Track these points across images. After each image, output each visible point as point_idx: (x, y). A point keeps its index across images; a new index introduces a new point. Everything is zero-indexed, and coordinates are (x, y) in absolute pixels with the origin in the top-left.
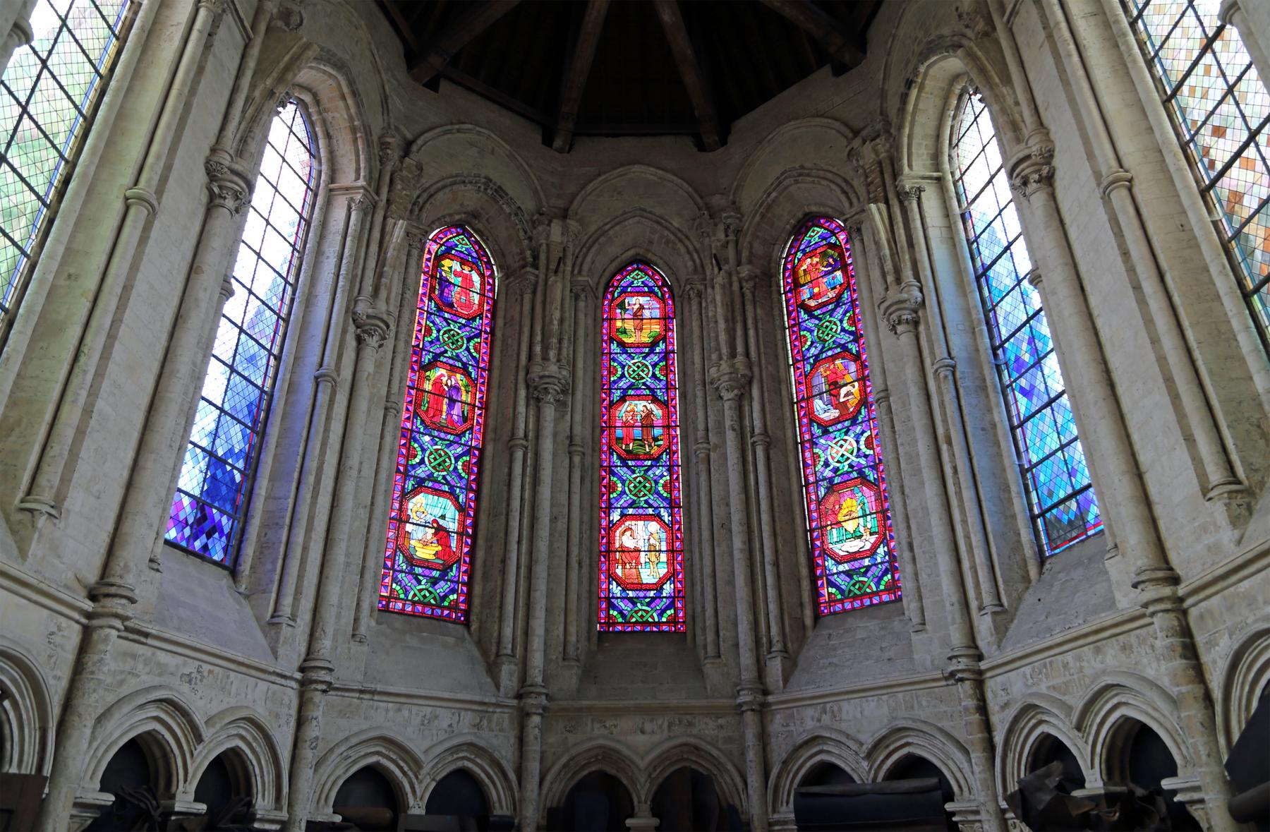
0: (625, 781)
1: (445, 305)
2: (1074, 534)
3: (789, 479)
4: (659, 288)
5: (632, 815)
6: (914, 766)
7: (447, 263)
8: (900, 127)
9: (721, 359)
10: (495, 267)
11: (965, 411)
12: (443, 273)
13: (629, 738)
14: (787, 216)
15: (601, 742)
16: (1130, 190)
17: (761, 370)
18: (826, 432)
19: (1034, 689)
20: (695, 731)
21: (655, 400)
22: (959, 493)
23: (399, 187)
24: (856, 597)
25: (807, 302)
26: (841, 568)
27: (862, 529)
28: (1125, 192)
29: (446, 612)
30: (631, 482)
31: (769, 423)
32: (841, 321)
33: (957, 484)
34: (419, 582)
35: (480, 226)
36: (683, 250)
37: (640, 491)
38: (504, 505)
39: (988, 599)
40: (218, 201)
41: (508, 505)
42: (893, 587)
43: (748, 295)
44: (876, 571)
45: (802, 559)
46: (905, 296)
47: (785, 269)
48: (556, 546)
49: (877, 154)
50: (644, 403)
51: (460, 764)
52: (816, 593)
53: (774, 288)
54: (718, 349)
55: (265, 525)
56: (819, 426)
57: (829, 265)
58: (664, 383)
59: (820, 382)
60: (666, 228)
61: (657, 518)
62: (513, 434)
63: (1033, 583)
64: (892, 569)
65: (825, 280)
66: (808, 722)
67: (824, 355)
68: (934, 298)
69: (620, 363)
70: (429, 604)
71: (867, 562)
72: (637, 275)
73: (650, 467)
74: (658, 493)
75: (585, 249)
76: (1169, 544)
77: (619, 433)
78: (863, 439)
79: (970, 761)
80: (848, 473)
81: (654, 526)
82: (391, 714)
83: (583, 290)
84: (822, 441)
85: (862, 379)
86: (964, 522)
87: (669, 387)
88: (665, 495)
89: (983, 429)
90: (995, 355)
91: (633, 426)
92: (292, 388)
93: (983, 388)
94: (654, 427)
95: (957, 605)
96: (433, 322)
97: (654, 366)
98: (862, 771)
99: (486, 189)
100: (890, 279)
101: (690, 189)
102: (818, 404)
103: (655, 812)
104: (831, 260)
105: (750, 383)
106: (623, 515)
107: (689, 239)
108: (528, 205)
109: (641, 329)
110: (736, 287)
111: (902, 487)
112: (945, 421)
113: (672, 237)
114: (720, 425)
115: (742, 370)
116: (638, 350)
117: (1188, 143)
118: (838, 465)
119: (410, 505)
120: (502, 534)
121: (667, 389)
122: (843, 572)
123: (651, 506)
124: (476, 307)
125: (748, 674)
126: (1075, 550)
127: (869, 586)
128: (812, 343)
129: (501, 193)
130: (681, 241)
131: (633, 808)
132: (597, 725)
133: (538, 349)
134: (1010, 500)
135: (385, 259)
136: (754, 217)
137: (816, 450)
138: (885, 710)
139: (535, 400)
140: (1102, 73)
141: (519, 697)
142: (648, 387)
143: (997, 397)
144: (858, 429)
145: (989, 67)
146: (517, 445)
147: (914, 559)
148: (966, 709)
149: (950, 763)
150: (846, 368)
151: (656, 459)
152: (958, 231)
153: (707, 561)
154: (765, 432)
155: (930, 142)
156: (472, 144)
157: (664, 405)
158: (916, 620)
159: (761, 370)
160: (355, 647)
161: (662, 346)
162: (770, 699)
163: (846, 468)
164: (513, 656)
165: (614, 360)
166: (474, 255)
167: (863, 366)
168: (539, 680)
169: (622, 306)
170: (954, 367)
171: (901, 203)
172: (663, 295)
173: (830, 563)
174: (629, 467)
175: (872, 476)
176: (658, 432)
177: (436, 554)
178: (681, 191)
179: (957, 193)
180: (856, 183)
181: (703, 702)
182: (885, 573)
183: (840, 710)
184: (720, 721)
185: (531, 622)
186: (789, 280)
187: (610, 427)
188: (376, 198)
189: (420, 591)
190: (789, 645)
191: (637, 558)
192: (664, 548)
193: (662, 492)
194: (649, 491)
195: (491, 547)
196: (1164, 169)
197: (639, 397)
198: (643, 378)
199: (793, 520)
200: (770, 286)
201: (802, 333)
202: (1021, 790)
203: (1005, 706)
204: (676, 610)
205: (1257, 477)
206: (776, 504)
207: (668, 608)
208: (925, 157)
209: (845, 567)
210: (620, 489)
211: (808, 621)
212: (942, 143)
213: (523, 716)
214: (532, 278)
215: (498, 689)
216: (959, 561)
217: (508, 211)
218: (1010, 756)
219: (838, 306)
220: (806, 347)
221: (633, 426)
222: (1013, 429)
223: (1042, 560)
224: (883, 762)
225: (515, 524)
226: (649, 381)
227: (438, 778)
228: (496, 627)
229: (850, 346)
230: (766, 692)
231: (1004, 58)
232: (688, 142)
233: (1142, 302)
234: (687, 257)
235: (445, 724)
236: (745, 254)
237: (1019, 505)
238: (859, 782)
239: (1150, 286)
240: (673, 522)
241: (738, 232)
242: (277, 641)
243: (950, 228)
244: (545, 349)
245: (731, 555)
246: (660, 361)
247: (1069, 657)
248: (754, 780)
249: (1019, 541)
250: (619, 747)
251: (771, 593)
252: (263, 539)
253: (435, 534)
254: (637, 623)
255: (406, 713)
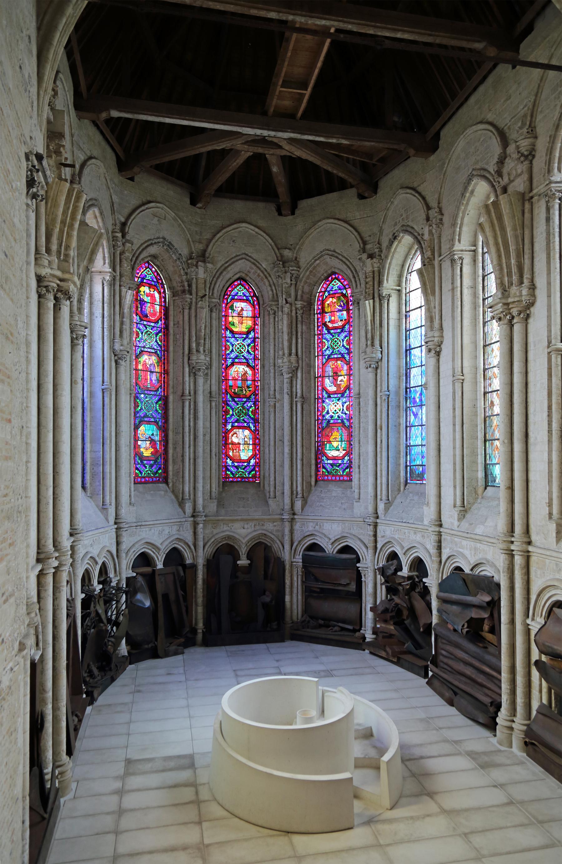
0: (236, 547)
1: (144, 316)
2: (419, 479)
3: (310, 418)
4: (252, 297)
5: (239, 559)
6: (347, 549)
7: (142, 289)
8: (387, 257)
9: (284, 355)
10: (165, 286)
11: (390, 417)
12: (141, 297)
13: (238, 531)
14: (322, 270)
15: (227, 533)
16: (462, 383)
17: (302, 362)
18: (329, 397)
19: (393, 536)
20: (265, 528)
21: (248, 365)
22: (381, 452)
23: (126, 265)
24: (333, 476)
25: (327, 323)
26: (329, 462)
27: (340, 447)
28: (460, 385)
29: (158, 479)
30: (236, 410)
31: (304, 390)
32: (343, 341)
33: (381, 448)
34: (146, 467)
35: (158, 263)
36: (267, 283)
37: (241, 414)
38: (181, 428)
39: (384, 498)
40: (75, 341)
41: (183, 429)
42: (349, 475)
43: (299, 317)
44: (344, 467)
45: (313, 456)
46: (374, 355)
47: (318, 300)
48: (205, 448)
49: (373, 267)
50: (243, 367)
51: (173, 546)
52: (317, 470)
53: (312, 312)
54: (283, 349)
55: (92, 464)
56: (327, 393)
57: (340, 306)
58: (253, 356)
59: (329, 370)
60: (258, 267)
61: (248, 428)
62: (183, 393)
63: (401, 492)
64: (350, 466)
65: (338, 314)
66: (310, 528)
67: (333, 356)
68: (386, 359)
69: (231, 343)
70: (151, 477)
71: (340, 462)
72: (240, 288)
73: (245, 402)
74: (249, 415)
75: (215, 279)
76: (442, 513)
77: (231, 383)
78: (345, 405)
79: (368, 551)
80: (337, 419)
81: (247, 432)
82: (148, 532)
83: (215, 306)
84: (327, 401)
85: (349, 375)
86: (381, 464)
87: (255, 358)
88: (252, 416)
89: (395, 426)
90: (406, 391)
91: (237, 380)
92: (92, 394)
93: (399, 407)
94: (247, 380)
95: (373, 497)
96: (139, 329)
97: (248, 345)
98: (330, 549)
99: (163, 246)
100: (369, 343)
101: (273, 244)
102: (327, 382)
103: (249, 557)
104: (342, 303)
105: (297, 369)
106: (232, 426)
107: (270, 276)
108: (185, 252)
109: (242, 323)
110: (294, 312)
111: (359, 440)
112: (381, 419)
113: (262, 275)
114: (282, 389)
115: (295, 364)
116: (240, 336)
117: (486, 369)
118: (333, 414)
119: (139, 432)
120: (181, 443)
121: (254, 359)
122: (330, 464)
123: (245, 422)
124: (158, 314)
125: (287, 507)
126: (418, 486)
127: (340, 472)
128: (328, 348)
129: (171, 247)
130: (266, 277)
131: (240, 557)
132: (225, 526)
133: (194, 345)
134: (400, 457)
135: (123, 313)
136: (306, 271)
137: (324, 404)
138: (340, 528)
139: (194, 373)
140: (466, 322)
141: (193, 516)
142: (245, 358)
143: (403, 413)
144: (344, 400)
145: (428, 284)
146: (186, 399)
147: (360, 472)
148: (369, 535)
149: (361, 550)
150: (342, 367)
151: (248, 398)
152: (402, 324)
153: (272, 455)
154: (302, 397)
155: (399, 268)
156: (155, 215)
157: (253, 368)
158: (356, 496)
159: (302, 362)
160: (132, 508)
161: (252, 335)
162: (296, 517)
163: (336, 417)
164: (190, 499)
165: (228, 341)
166: (155, 280)
167: (350, 369)
168: (201, 509)
169: (232, 308)
170: (389, 395)
171: (380, 300)
172: (254, 302)
173: (324, 458)
174: (235, 402)
175: (347, 424)
176: (249, 383)
177: (152, 453)
178: (267, 243)
179: (406, 300)
180: (360, 274)
181: (269, 517)
182: (347, 468)
183: (323, 525)
184: (275, 524)
185: (196, 484)
186: (320, 307)
187: (226, 379)
188: (115, 274)
189: (147, 471)
190: (305, 494)
191: (239, 447)
192: (251, 443)
193: (251, 415)
194: (245, 414)
195: (176, 448)
196: (476, 378)
197: (241, 363)
198: (242, 353)
199: (311, 437)
200: (310, 311)
201: (323, 340)
202: (383, 568)
203: (383, 537)
204: (256, 471)
205: (469, 506)
206: (304, 431)
207: (252, 471)
208: (395, 276)
209: (330, 462)
210: (231, 413)
211: (313, 483)
212: (404, 271)
213: (195, 525)
214: (189, 300)
215: (185, 514)
216: (376, 479)
217: (175, 258)
218: (381, 553)
219: (342, 331)
220: (325, 349)
221: (237, 380)
222: (406, 427)
223: (406, 483)
224: (337, 546)
225: (187, 439)
226: (245, 354)
227: (166, 552)
228: (181, 486)
229: (346, 356)
230: (294, 514)
231: (435, 279)
232: (272, 207)
233: (454, 431)
234: (269, 288)
235: (167, 532)
236: (300, 293)
237: (402, 461)
238: (327, 552)
239: (458, 428)
240: (256, 430)
241: (297, 278)
242: (107, 515)
243: (399, 320)
244: (198, 344)
245: (283, 454)
246: (251, 343)
247: (406, 531)
248: (287, 547)
249: (400, 475)
250: (235, 535)
251: (299, 473)
252: (93, 471)
253: (150, 444)
254: (238, 477)
255: (153, 531)
